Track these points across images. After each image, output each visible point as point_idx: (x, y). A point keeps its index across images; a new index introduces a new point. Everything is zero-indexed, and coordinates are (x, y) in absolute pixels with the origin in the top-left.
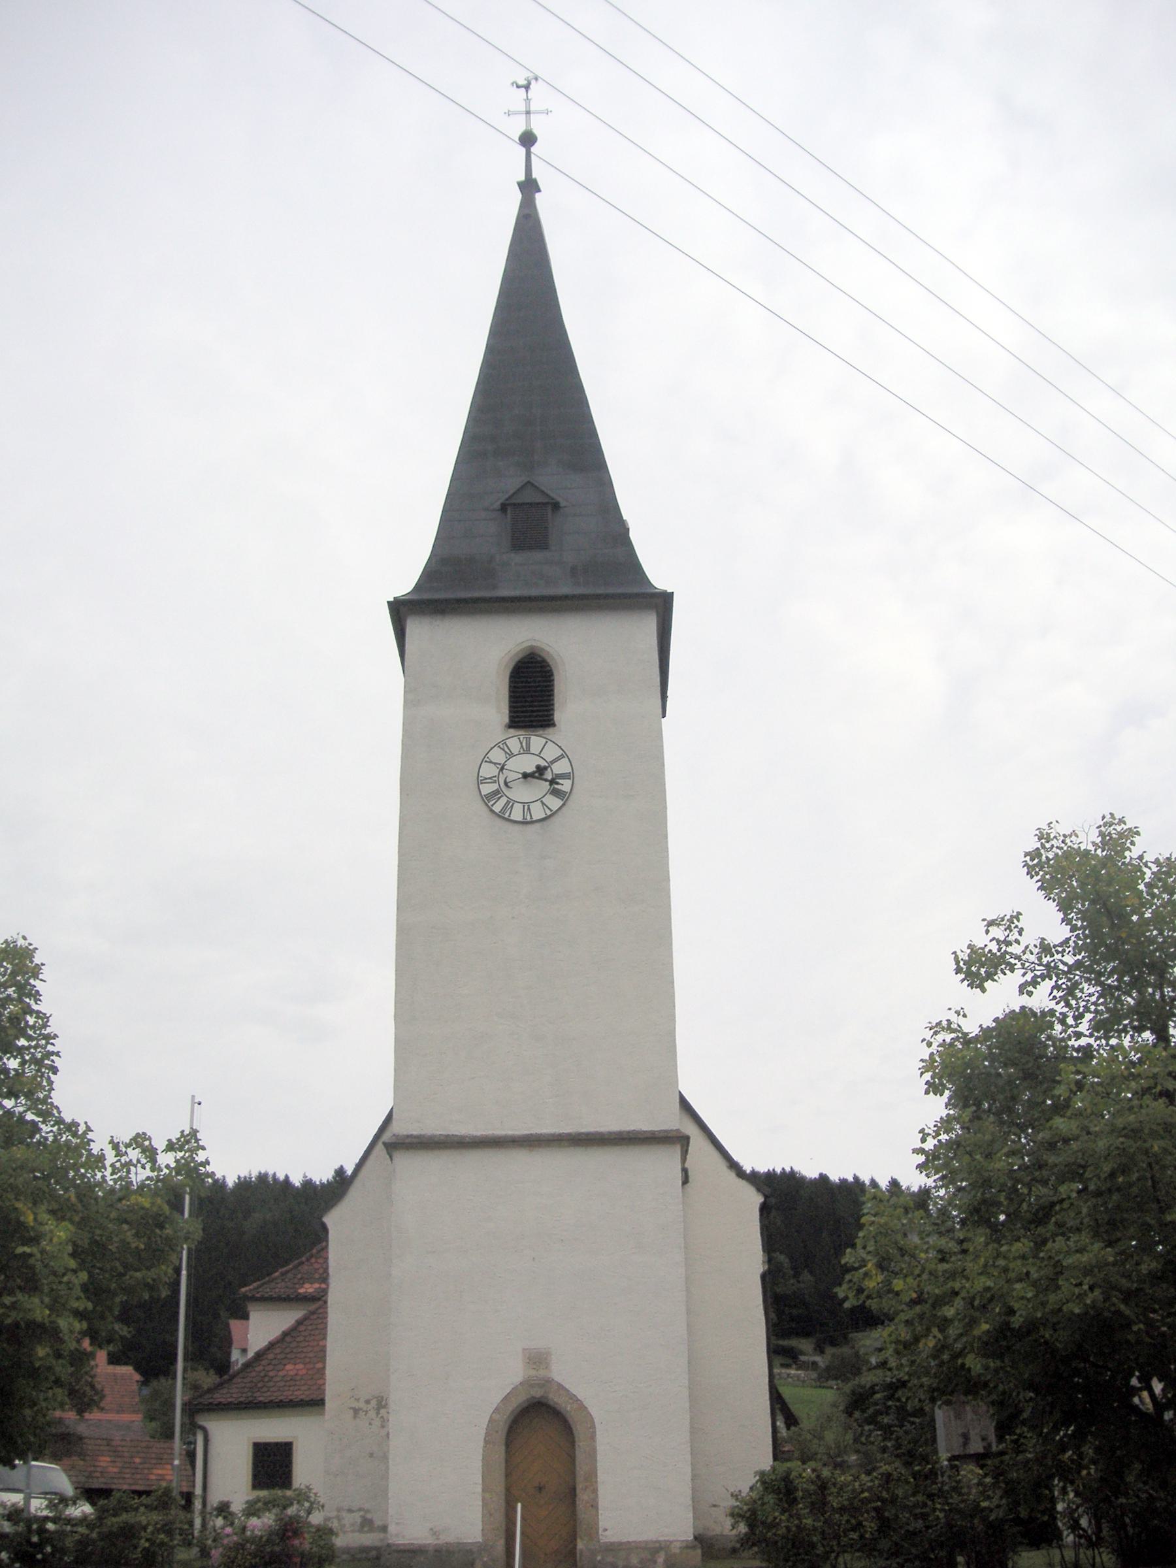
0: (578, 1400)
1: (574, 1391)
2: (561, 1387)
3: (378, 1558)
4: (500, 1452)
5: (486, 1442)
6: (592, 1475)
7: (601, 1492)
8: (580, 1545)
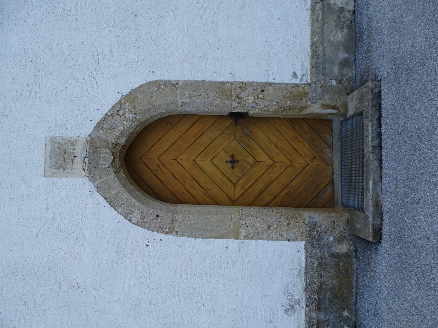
0: (120, 103)
1: (105, 109)
2: (100, 126)
3: (374, 147)
4: (188, 213)
5: (170, 232)
6: (222, 89)
7: (246, 79)
8: (316, 109)
